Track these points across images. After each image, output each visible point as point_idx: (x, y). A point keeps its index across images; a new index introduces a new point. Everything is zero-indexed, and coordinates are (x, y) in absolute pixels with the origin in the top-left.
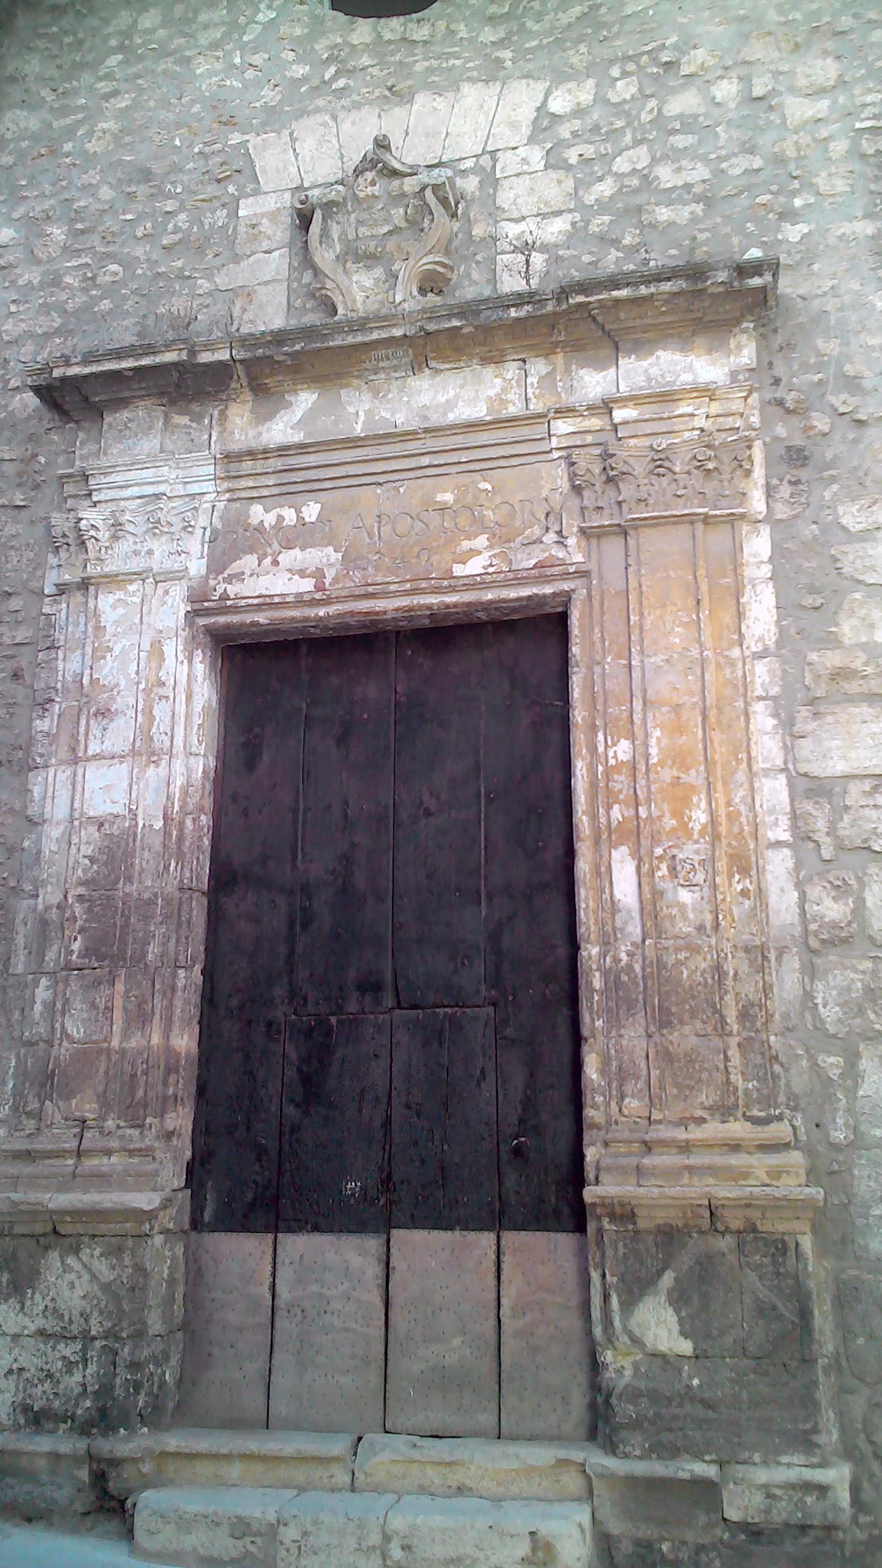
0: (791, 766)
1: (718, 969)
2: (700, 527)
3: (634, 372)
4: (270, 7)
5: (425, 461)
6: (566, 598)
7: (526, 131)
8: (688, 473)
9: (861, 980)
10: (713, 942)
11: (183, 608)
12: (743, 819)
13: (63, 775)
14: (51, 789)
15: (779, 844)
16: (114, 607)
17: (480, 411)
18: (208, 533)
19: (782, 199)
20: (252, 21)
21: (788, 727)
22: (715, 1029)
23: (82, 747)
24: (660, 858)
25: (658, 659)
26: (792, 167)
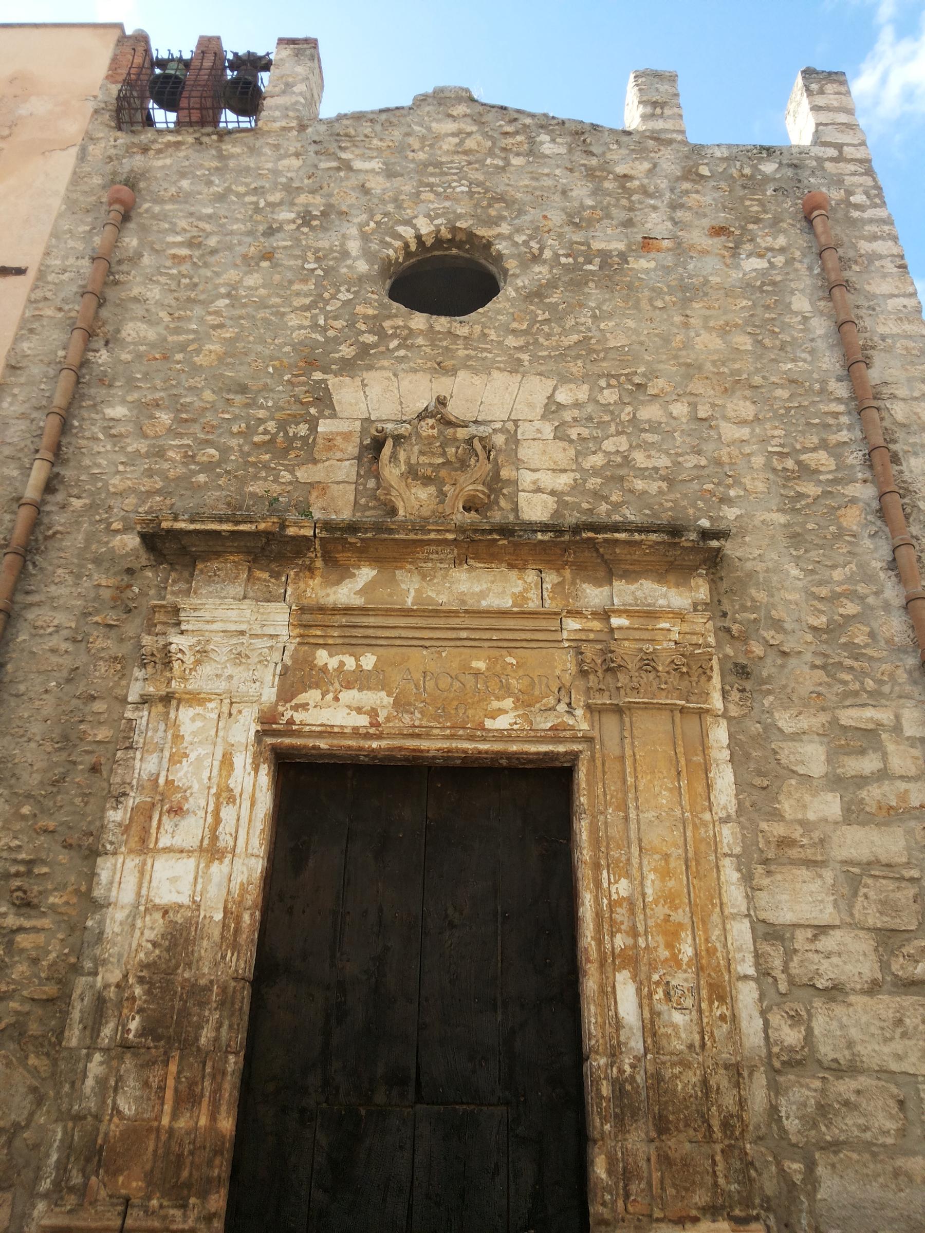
0: (752, 913)
1: (705, 1082)
2: (677, 715)
3: (624, 592)
4: (348, 291)
5: (464, 634)
6: (575, 756)
7: (540, 411)
8: (668, 672)
9: (814, 1097)
10: (701, 1059)
11: (254, 727)
12: (719, 954)
13: (132, 863)
14: (118, 875)
15: (746, 977)
16: (193, 720)
17: (507, 603)
18: (279, 668)
19: (721, 489)
20: (334, 297)
21: (747, 878)
22: (705, 1137)
23: (153, 839)
24: (658, 983)
25: (650, 815)
26: (727, 469)
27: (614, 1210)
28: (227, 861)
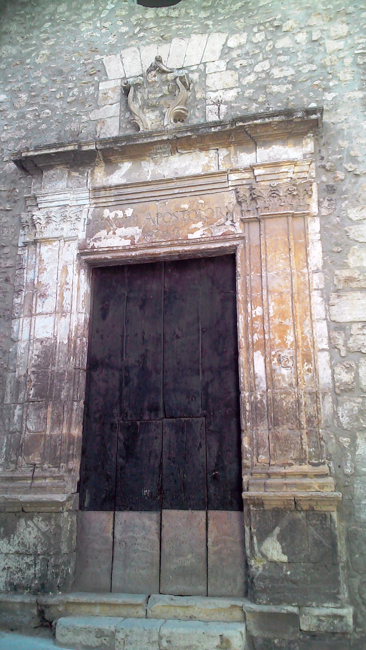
0: (328, 318)
1: (298, 402)
2: (290, 218)
3: (263, 154)
4: (112, 3)
5: (176, 191)
6: (235, 248)
7: (218, 54)
8: (286, 196)
9: (357, 406)
10: (296, 391)
11: (76, 252)
12: (308, 340)
13: (26, 321)
15: (323, 350)
16: (47, 252)
17: (199, 171)
20: (105, 9)
21: (327, 300)
22: (297, 427)
23: (34, 310)
24: (274, 356)
25: (273, 273)
26: (328, 69)
27: (252, 462)
28: (68, 316)
